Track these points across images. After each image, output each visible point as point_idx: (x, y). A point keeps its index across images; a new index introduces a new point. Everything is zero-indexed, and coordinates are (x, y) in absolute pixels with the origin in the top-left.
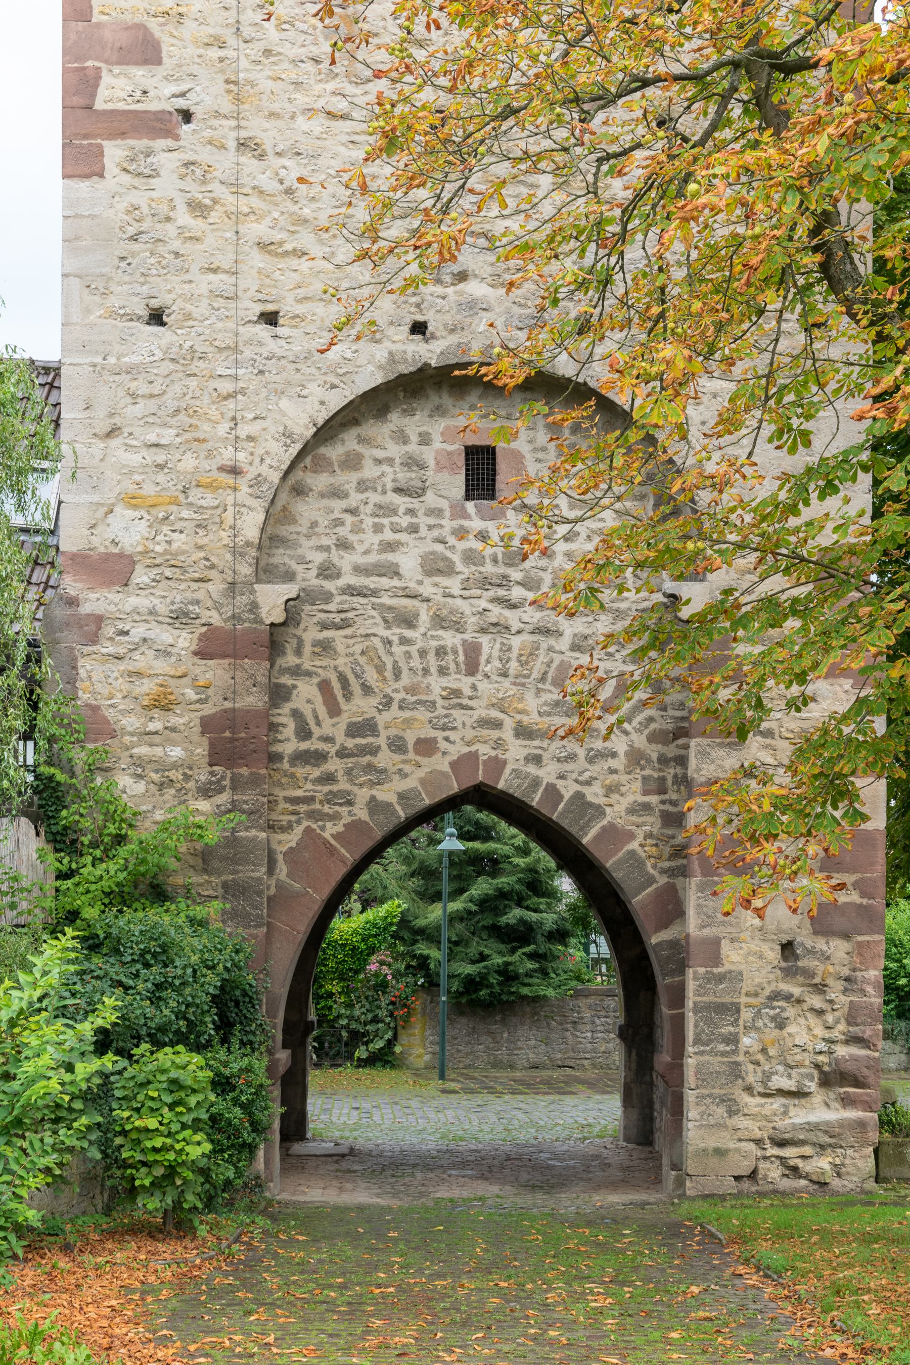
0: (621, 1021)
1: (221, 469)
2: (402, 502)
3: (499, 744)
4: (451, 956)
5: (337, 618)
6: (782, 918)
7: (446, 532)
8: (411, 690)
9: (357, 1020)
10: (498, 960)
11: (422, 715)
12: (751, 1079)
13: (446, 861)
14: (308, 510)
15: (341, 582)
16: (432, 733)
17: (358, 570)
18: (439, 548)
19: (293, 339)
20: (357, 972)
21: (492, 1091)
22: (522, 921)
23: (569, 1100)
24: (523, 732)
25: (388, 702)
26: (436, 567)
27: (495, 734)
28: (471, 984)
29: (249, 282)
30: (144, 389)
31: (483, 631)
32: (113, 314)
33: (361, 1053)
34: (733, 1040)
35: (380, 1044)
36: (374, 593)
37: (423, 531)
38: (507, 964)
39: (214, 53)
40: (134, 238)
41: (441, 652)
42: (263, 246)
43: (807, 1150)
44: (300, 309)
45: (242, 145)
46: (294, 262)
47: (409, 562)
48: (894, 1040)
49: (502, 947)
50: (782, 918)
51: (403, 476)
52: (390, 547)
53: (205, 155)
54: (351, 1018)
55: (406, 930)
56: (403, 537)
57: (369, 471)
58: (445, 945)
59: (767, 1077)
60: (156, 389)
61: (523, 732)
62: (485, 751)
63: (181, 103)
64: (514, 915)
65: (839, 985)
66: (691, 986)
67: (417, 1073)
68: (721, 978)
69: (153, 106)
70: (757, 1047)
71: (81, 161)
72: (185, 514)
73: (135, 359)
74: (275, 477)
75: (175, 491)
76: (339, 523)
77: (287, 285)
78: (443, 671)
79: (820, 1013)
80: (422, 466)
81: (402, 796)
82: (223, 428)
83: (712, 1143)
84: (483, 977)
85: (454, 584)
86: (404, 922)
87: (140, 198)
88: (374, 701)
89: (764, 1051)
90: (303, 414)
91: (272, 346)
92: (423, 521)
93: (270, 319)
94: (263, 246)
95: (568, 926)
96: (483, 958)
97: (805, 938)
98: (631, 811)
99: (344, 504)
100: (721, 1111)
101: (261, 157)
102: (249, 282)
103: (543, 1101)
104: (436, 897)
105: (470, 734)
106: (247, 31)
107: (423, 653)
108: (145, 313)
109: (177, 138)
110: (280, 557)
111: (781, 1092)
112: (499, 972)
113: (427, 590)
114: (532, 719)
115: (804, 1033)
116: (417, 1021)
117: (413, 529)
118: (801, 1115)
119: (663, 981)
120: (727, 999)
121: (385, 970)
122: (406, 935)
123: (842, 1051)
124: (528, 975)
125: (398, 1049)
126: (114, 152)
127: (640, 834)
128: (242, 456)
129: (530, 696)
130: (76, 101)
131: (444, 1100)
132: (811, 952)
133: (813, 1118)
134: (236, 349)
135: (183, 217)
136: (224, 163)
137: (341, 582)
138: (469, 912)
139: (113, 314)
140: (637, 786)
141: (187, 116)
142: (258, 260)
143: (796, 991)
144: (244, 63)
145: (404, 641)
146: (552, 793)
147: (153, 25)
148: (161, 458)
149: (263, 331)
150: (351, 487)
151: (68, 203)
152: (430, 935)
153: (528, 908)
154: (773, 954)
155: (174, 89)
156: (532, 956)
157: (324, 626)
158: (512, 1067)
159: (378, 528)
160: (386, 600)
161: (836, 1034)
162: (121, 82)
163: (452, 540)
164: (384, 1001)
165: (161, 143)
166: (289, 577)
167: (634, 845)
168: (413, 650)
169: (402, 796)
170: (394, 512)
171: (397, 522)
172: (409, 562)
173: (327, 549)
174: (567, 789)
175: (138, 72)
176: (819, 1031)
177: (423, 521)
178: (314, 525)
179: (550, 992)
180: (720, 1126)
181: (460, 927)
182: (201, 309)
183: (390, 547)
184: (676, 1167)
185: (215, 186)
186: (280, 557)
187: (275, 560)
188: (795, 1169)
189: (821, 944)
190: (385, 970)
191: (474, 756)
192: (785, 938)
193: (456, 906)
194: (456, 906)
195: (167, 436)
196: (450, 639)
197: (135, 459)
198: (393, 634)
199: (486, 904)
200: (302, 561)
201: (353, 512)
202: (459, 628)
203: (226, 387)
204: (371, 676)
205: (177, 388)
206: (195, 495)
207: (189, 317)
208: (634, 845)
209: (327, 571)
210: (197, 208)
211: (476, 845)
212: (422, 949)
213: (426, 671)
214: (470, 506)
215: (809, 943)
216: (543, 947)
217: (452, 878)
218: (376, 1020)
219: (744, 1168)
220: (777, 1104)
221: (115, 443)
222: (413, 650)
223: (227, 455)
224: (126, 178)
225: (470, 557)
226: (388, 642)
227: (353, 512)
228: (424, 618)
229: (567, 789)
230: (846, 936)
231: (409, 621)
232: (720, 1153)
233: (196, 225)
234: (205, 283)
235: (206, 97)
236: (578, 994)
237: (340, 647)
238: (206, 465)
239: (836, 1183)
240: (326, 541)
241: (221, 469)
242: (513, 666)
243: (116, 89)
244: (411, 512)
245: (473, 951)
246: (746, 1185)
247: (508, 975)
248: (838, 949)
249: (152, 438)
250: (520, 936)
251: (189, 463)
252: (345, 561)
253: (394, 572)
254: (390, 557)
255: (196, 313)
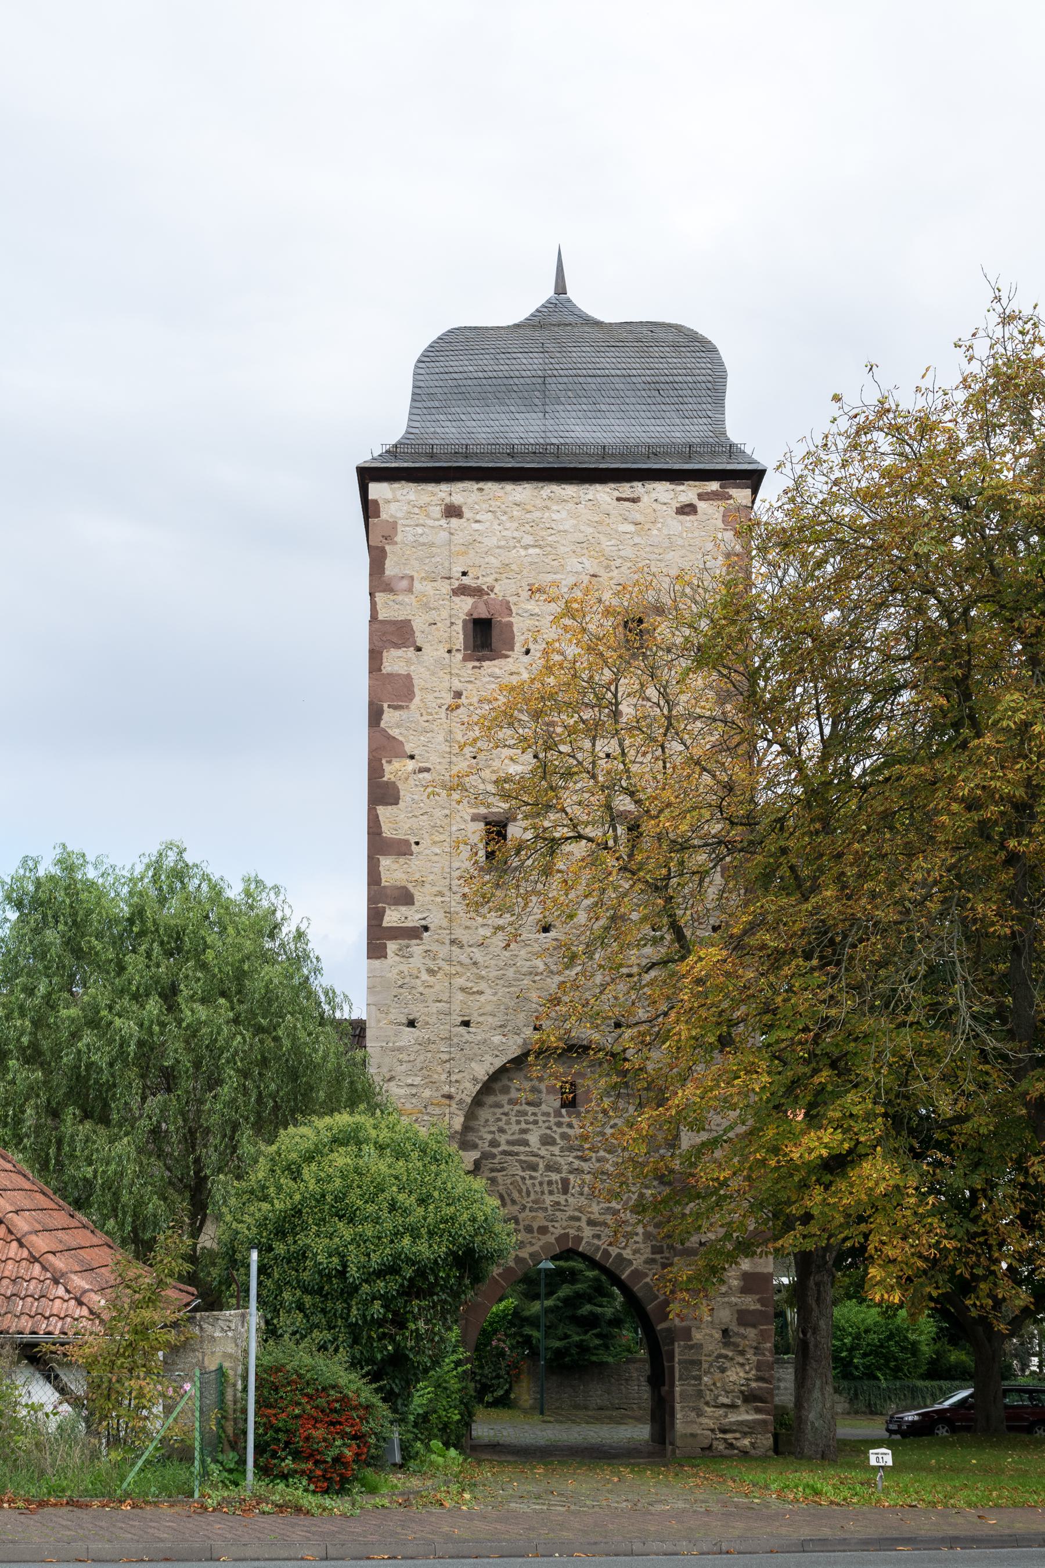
0: (649, 1373)
1: (443, 1096)
2: (530, 1109)
3: (579, 1229)
4: (547, 1336)
5: (499, 1167)
6: (725, 1316)
7: (552, 1124)
8: (535, 1202)
9: (486, 1377)
10: (577, 1338)
11: (541, 1214)
12: (708, 1398)
13: (543, 1275)
14: (484, 1114)
15: (500, 1149)
16: (546, 1224)
17: (509, 1143)
18: (548, 1132)
19: (476, 1034)
20: (486, 1346)
21: (574, 1422)
22: (591, 1313)
23: (623, 1427)
24: (591, 1223)
25: (524, 1208)
26: (547, 1141)
27: (577, 1224)
28: (559, 1353)
29: (456, 1007)
30: (406, 1058)
31: (570, 1172)
32: (391, 1023)
33: (488, 1398)
34: (699, 1378)
35: (501, 1393)
36: (517, 1154)
37: (541, 1124)
38: (582, 1341)
39: (439, 899)
40: (401, 987)
41: (550, 1183)
42: (462, 989)
43: (738, 1435)
44: (480, 1019)
45: (453, 942)
46: (477, 997)
47: (533, 1139)
48: (840, 1394)
49: (579, 1330)
50: (725, 1316)
51: (531, 1097)
52: (524, 1131)
53: (435, 947)
54: (482, 1375)
55: (517, 1318)
56: (531, 1126)
57: (514, 1094)
58: (543, 1328)
59: (717, 1397)
60: (412, 1058)
61: (591, 1223)
62: (572, 1232)
63: (423, 923)
64: (587, 1309)
65: (752, 1351)
66: (677, 1351)
67: (525, 1411)
68: (692, 1347)
69: (409, 924)
70: (711, 1382)
71: (376, 950)
72: (426, 1118)
73: (402, 1044)
74: (469, 1100)
75: (421, 1107)
76: (499, 1120)
77: (474, 1007)
78: (551, 1193)
79: (742, 1365)
80: (540, 1092)
81: (531, 1255)
82: (444, 1077)
83: (689, 1431)
84: (567, 1349)
85: (556, 1150)
86: (516, 1313)
87: (404, 968)
88: (517, 1207)
89: (714, 1384)
90: (482, 1070)
91: (467, 1037)
92: (541, 1118)
93: (466, 1024)
94: (462, 989)
95: (622, 1316)
96: (566, 1337)
97: (734, 1327)
98: (646, 1262)
99: (501, 1111)
100: (693, 1414)
101: (461, 947)
102: (456, 1007)
103: (605, 1427)
104: (536, 1297)
105: (565, 1224)
106: (455, 888)
107: (541, 1184)
108: (405, 1021)
109: (421, 939)
110: (471, 1137)
111: (724, 1405)
112: (577, 1346)
113: (543, 1152)
114: (595, 1216)
115: (735, 1375)
116: (524, 1377)
117: (536, 1122)
118: (733, 1417)
119: (665, 1349)
120: (695, 1358)
121: (502, 1345)
122: (517, 1322)
123: (754, 1385)
124: (596, 1348)
125: (512, 1396)
126: (392, 946)
127: (651, 1273)
128: (453, 1090)
129: (594, 1205)
130: (373, 922)
131: (544, 1426)
132: (737, 1334)
133: (740, 1418)
134: (450, 1039)
135: (425, 976)
136: (443, 951)
137: (500, 1149)
138: (557, 1307)
139: (391, 1023)
140: (649, 1250)
141: (426, 929)
142: (460, 996)
143: (730, 1354)
144: (453, 903)
145: (531, 1178)
146: (606, 1253)
147: (410, 886)
148: (414, 1091)
149: (462, 1030)
150: (505, 1102)
151: (370, 970)
152: (533, 1322)
153: (595, 1305)
154: (718, 1335)
155: (420, 916)
156: (598, 1336)
157: (492, 1170)
158: (586, 1408)
159: (518, 1122)
160: (522, 1158)
161: (750, 1376)
162: (395, 913)
163: (555, 1128)
164: (503, 1364)
165: (414, 942)
166: (475, 1146)
167: (648, 1280)
168: (536, 1182)
169: (531, 1255)
170: (526, 1114)
171: (532, 1126)
172: (533, 1139)
173: (493, 1133)
174: (614, 1251)
175: (403, 909)
176: (742, 1374)
177: (541, 1118)
178: (487, 1121)
179: (610, 1360)
180: (693, 1422)
181: (551, 1316)
182: (433, 1020)
183: (524, 1131)
184: (672, 1444)
185: (440, 961)
186: (471, 1137)
187: (468, 1138)
188: (731, 1444)
189: (742, 1330)
190: (502, 1345)
191: (567, 1235)
192: (724, 1327)
193: (549, 1303)
194: (549, 1303)
195: (417, 1080)
196: (555, 1177)
197: (402, 1092)
198: (527, 1174)
199: (567, 1301)
200: (481, 1138)
201: (506, 1114)
202: (558, 1171)
203: (445, 1057)
204: (516, 1195)
205: (422, 1058)
206: (430, 1109)
207: (427, 1023)
208: (648, 1280)
209: (494, 1143)
210: (431, 972)
211: (561, 1263)
212: (528, 1331)
213: (543, 1193)
214: (563, 1111)
215: (736, 1329)
216: (605, 1330)
217: (546, 1285)
218: (498, 1377)
219: (706, 1443)
220: (721, 1411)
221: (392, 1084)
222: (536, 1182)
223: (446, 1089)
224: (397, 958)
225: (564, 1136)
226: (523, 1178)
227: (506, 1114)
228: (541, 1166)
229: (614, 1251)
230: (754, 1326)
231: (534, 1168)
232: (693, 1436)
233: (431, 980)
234: (435, 1007)
235: (436, 919)
236: (629, 1361)
237: (500, 1181)
238: (435, 1094)
239: (753, 1452)
240: (493, 1129)
241: (443, 1096)
242: (586, 1189)
243: (393, 917)
244: (534, 1114)
245: (560, 1332)
246: (707, 1452)
247: (583, 1348)
248: (751, 1333)
249: (409, 1081)
250: (591, 1322)
251: (427, 1093)
252: (502, 1139)
253: (526, 1143)
254: (524, 1136)
255: (431, 1021)
